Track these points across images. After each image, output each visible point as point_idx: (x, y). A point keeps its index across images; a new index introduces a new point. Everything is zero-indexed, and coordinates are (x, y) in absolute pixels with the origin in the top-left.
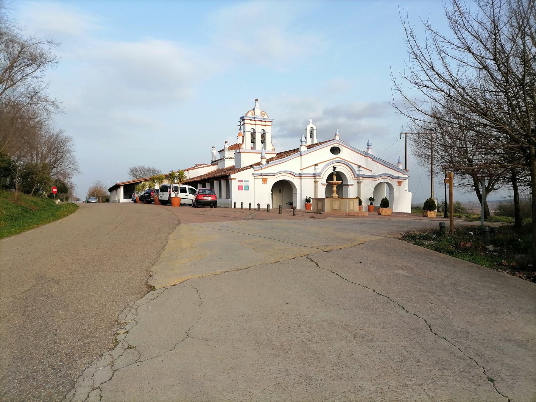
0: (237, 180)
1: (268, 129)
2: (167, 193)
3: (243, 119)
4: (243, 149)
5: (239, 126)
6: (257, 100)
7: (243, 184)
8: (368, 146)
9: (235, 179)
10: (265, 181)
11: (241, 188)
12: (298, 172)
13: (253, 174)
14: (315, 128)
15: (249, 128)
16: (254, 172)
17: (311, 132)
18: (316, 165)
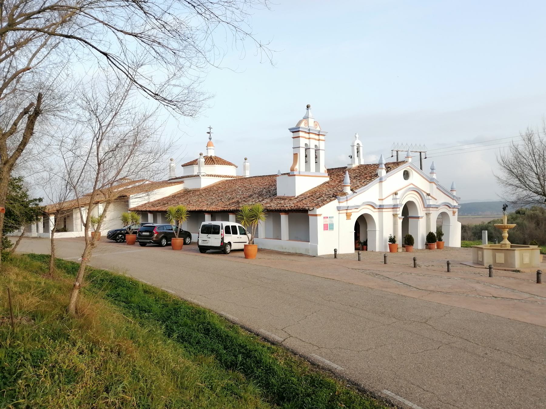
0: (322, 216)
1: (322, 145)
2: (219, 236)
3: (295, 131)
4: (296, 170)
5: (208, 133)
6: (308, 107)
7: (328, 221)
8: (432, 169)
9: (320, 215)
10: (348, 216)
11: (326, 227)
12: (378, 203)
13: (338, 207)
14: (361, 145)
15: (303, 142)
16: (338, 205)
17: (358, 149)
18: (396, 194)
